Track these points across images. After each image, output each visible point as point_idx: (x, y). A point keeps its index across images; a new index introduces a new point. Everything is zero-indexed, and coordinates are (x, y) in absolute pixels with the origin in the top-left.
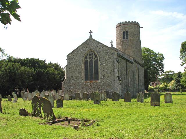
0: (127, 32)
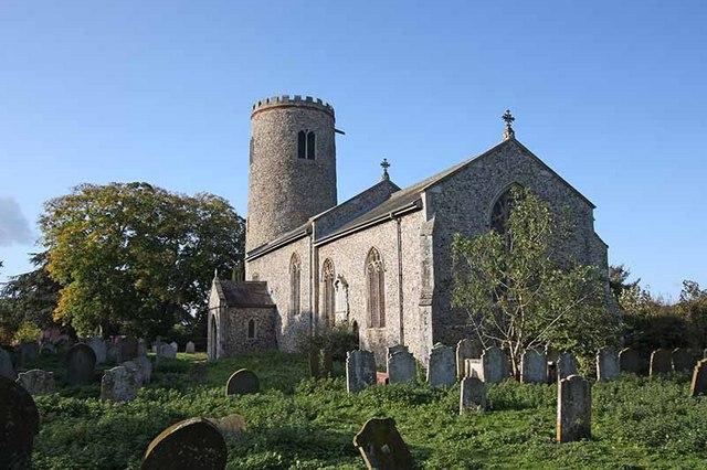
0: (312, 136)
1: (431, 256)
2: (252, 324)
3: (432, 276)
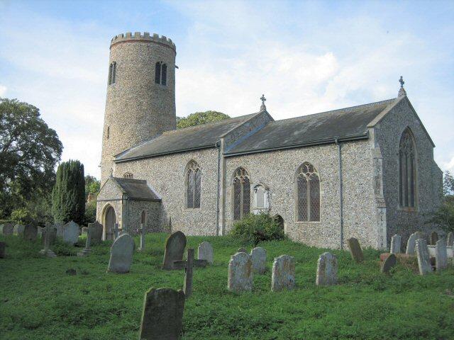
1: (381, 173)
3: (382, 187)
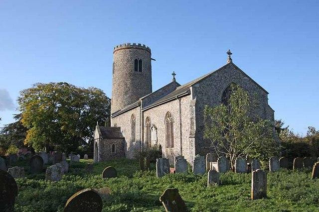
0: (141, 61)
1: (194, 115)
2: (113, 146)
3: (195, 124)
